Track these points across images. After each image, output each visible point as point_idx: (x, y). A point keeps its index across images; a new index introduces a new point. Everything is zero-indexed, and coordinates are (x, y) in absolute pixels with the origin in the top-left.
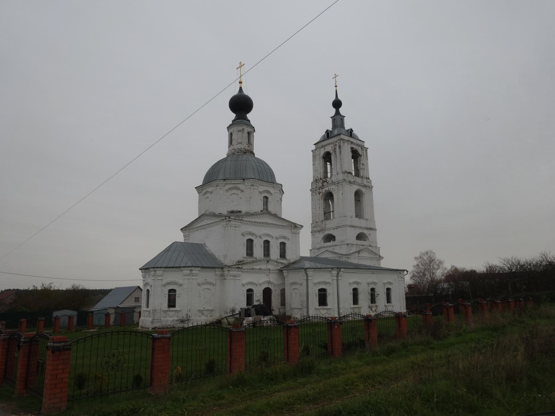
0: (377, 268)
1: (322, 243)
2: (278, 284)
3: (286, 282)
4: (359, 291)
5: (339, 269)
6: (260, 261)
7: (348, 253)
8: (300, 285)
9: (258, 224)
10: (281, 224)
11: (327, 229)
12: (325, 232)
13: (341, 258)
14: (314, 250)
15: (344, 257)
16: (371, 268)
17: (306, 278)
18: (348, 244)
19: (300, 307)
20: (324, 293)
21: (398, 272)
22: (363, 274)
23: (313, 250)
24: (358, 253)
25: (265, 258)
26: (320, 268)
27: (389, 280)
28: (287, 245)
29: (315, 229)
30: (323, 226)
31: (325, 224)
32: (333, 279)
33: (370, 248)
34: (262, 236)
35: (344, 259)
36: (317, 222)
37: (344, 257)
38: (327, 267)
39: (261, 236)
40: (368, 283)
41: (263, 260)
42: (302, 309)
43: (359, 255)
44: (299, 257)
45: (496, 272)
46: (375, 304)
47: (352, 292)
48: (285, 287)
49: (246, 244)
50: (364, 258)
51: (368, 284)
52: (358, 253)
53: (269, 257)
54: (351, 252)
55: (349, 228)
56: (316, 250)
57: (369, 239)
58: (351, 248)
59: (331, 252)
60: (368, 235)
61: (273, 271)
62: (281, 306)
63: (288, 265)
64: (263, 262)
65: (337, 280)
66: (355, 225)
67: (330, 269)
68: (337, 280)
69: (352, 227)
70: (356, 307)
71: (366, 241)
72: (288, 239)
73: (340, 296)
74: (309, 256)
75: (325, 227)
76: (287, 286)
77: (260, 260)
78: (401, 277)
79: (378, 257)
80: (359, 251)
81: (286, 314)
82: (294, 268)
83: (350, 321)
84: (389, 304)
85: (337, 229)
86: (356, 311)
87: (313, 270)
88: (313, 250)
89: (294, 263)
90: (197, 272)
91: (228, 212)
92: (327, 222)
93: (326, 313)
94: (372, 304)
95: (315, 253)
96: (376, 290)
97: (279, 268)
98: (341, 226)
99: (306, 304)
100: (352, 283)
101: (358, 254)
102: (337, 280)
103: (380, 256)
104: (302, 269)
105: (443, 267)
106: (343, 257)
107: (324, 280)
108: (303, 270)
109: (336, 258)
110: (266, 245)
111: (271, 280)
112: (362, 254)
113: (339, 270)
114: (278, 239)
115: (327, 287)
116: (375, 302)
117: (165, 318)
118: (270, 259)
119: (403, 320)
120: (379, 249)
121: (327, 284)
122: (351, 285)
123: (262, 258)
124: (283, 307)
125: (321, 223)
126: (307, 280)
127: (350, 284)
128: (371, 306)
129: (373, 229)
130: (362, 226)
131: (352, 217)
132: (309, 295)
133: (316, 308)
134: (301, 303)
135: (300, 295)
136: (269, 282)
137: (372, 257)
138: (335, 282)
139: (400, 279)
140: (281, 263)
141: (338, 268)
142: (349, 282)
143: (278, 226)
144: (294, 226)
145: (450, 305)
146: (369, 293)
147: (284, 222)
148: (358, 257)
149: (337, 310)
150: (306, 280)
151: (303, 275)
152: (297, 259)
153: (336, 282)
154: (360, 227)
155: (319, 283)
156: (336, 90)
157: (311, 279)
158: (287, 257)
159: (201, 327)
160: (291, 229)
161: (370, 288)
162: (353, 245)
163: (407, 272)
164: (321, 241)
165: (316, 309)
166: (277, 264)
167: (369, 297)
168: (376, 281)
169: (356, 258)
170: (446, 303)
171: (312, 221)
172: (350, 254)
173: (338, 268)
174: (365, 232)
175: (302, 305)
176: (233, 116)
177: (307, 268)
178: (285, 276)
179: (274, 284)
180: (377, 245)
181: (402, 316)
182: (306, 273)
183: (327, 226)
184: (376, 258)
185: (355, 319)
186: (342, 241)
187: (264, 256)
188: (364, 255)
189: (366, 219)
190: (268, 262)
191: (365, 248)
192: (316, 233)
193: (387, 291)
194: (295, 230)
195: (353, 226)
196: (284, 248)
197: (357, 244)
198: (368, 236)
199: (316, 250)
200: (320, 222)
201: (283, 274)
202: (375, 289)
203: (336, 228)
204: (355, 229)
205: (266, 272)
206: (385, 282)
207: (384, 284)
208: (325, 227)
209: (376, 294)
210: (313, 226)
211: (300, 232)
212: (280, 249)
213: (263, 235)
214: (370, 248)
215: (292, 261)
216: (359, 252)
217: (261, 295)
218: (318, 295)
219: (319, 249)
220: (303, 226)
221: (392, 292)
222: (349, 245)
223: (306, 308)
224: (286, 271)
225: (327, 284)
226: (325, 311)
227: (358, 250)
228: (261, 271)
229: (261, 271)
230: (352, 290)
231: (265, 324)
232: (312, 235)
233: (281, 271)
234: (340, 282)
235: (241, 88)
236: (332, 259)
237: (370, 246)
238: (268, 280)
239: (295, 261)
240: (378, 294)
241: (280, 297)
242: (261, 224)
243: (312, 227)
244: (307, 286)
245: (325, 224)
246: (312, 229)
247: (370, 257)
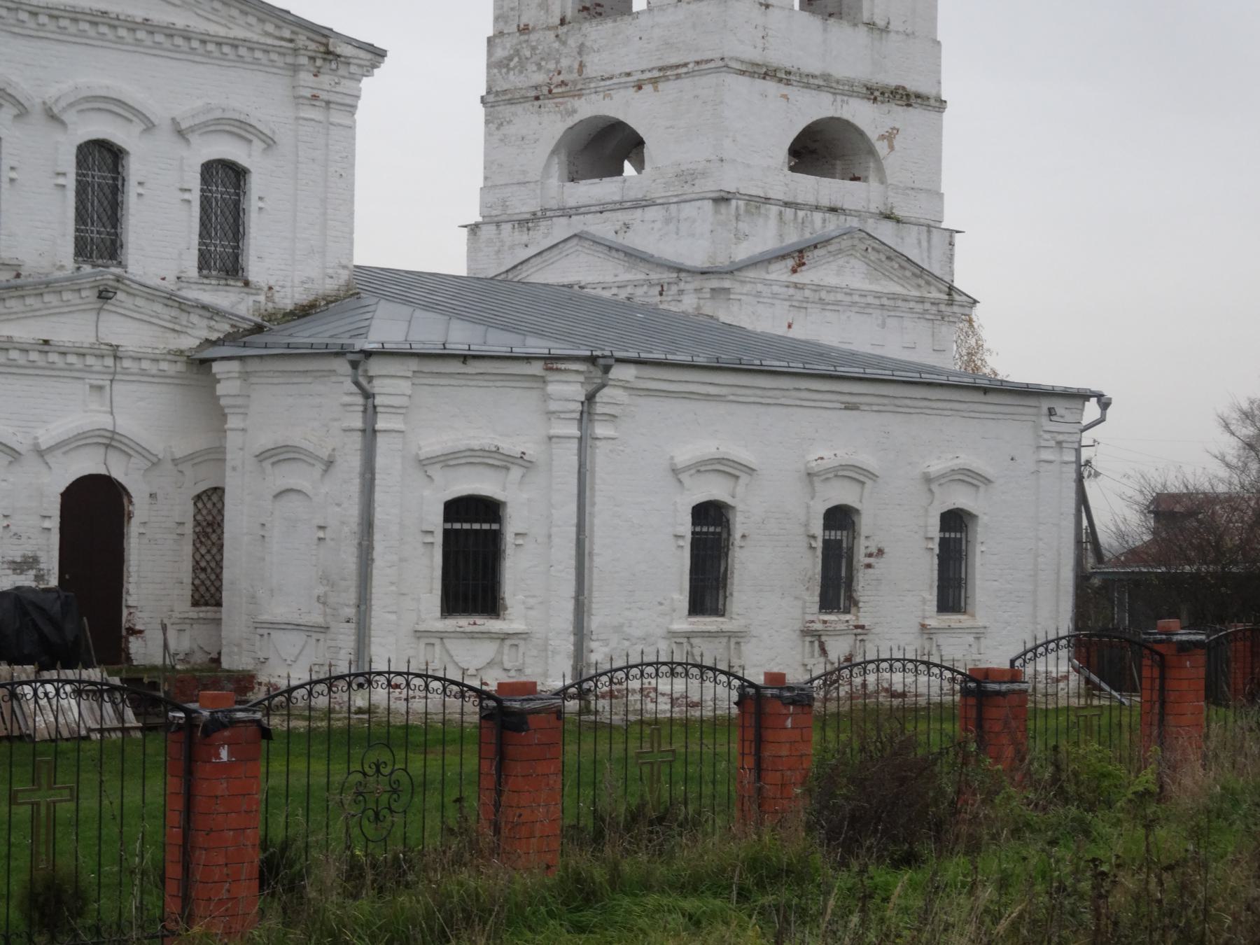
0: (886, 374)
1: (554, 182)
2: (178, 454)
3: (233, 441)
4: (740, 525)
5: (599, 364)
6: (45, 286)
7: (722, 261)
8: (320, 467)
9: (43, 19)
10: (213, 29)
11: (591, 79)
12: (577, 103)
13: (674, 289)
14: (493, 227)
15: (690, 284)
16: (842, 370)
17: (359, 424)
18: (722, 199)
19: (316, 618)
20: (486, 526)
21: (1032, 401)
22: (772, 409)
23: (488, 232)
24: (790, 263)
25: (87, 268)
26: (465, 358)
27: (967, 459)
28: (256, 185)
29: (515, 80)
30: (565, 63)
31: (581, 49)
32: (550, 438)
33: (885, 231)
34: (64, 110)
35: (688, 303)
36: (524, 30)
37: (689, 287)
38: (518, 351)
39: (55, 110)
40: (809, 474)
41: (73, 285)
42: (325, 629)
43: (796, 278)
44: (344, 275)
46: (848, 617)
47: (686, 527)
48: (224, 477)
49: (71, 182)
50: (831, 297)
51: (811, 483)
52: (790, 263)
53: (120, 264)
54: (742, 252)
55: (745, 80)
56: (507, 228)
57: (880, 170)
58: (744, 226)
59: (610, 248)
60: (882, 137)
61: (145, 365)
62: (195, 604)
63: (259, 329)
64: (67, 296)
65: (584, 443)
66: (787, 63)
67: (536, 368)
68: (584, 443)
69: (765, 76)
70: (713, 628)
71: (866, 180)
72: (270, 143)
73: (597, 550)
74: (464, 273)
75: (580, 72)
76: (234, 469)
77: (48, 284)
78: (1059, 443)
79: (935, 294)
80: (801, 251)
81: (226, 664)
82: (288, 346)
83: (656, 721)
84: (952, 619)
85: (661, 86)
86: (709, 652)
87: (413, 365)
88: (488, 232)
89: (304, 312)
90: (405, 386)
92: (597, 32)
93: (490, 664)
94: (826, 617)
95: (499, 251)
96: (865, 524)
97: (188, 342)
98: (685, 65)
99: (351, 596)
100: (688, 468)
101: (794, 271)
102: (580, 439)
103: (951, 289)
104: (337, 354)
106: (682, 285)
107: (481, 438)
108: (343, 366)
109: (640, 291)
110: (218, 191)
111: (127, 425)
112: (820, 273)
113: (599, 374)
114: (187, 141)
115: (504, 489)
116: (852, 603)
118: (118, 279)
119: (789, 723)
120: (951, 244)
121: (508, 469)
122: (680, 482)
123: (62, 267)
124: (206, 612)
125: (551, 35)
126: (370, 433)
127: (675, 471)
128: (818, 626)
129: (918, 96)
130: (841, 71)
131: (767, 6)
132: (377, 537)
133: (422, 627)
134: (320, 590)
135: (321, 534)
136: (111, 441)
137: (893, 297)
138: (568, 456)
139: (1046, 455)
140: (205, 307)
141: (592, 360)
142: (672, 458)
143: (195, 44)
144: (313, 46)
145: (1183, 636)
146: (814, 537)
147: (241, 20)
148: (791, 291)
149: (568, 645)
150: (364, 431)
151: (347, 399)
152: (329, 286)
153: (574, 460)
154: (826, 77)
155: (449, 460)
157: (400, 426)
158: (256, 269)
160: (295, 68)
161: (820, 508)
162: (759, 202)
163: (1104, 404)
164: (547, 166)
165: (419, 634)
166: (174, 313)
167: (813, 565)
168: (867, 459)
169: (775, 296)
170: (1162, 623)
171: (497, 19)
172: (733, 270)
173: (592, 360)
174: (861, 114)
175: (324, 603)
177: (368, 354)
178: (223, 402)
179: (143, 452)
180: (941, 212)
181: (779, 697)
182: (357, 383)
183: (596, 65)
184: (921, 300)
185: (696, 713)
186: (687, 176)
187: (83, 250)
188: (832, 280)
189: (871, 25)
190: (104, 295)
191: (848, 233)
192: (513, 108)
193: (942, 529)
194: (326, 80)
195: (769, 73)
196: (237, 204)
197: (790, 199)
198: (881, 148)
199: (507, 228)
200: (549, 28)
201: (214, 389)
202: (857, 511)
203: (654, 81)
204: (784, 89)
205: (88, 369)
206: (937, 466)
207: (928, 479)
208: (580, 72)
209: (862, 547)
210: (500, 53)
211: (358, 97)
212: (203, 208)
213: (71, 105)
214: (885, 231)
215: (288, 299)
216: (799, 256)
217: (47, 524)
218: (438, 539)
219: (526, 223)
220: (379, 54)
221: (980, 538)
222: (734, 202)
223: (353, 625)
224: (235, 366)
225: (508, 469)
226: (487, 650)
227: (793, 238)
228: (53, 357)
229: (53, 357)
230: (689, 519)
231: (40, 723)
232: (487, 122)
233: (204, 364)
234: (601, 458)
236: (607, 294)
237: (888, 217)
238: (104, 421)
239: (312, 298)
240: (881, 552)
241: (188, 549)
242: (63, 23)
243: (489, 66)
245: (581, 49)
246: (488, 73)
247: (878, 296)
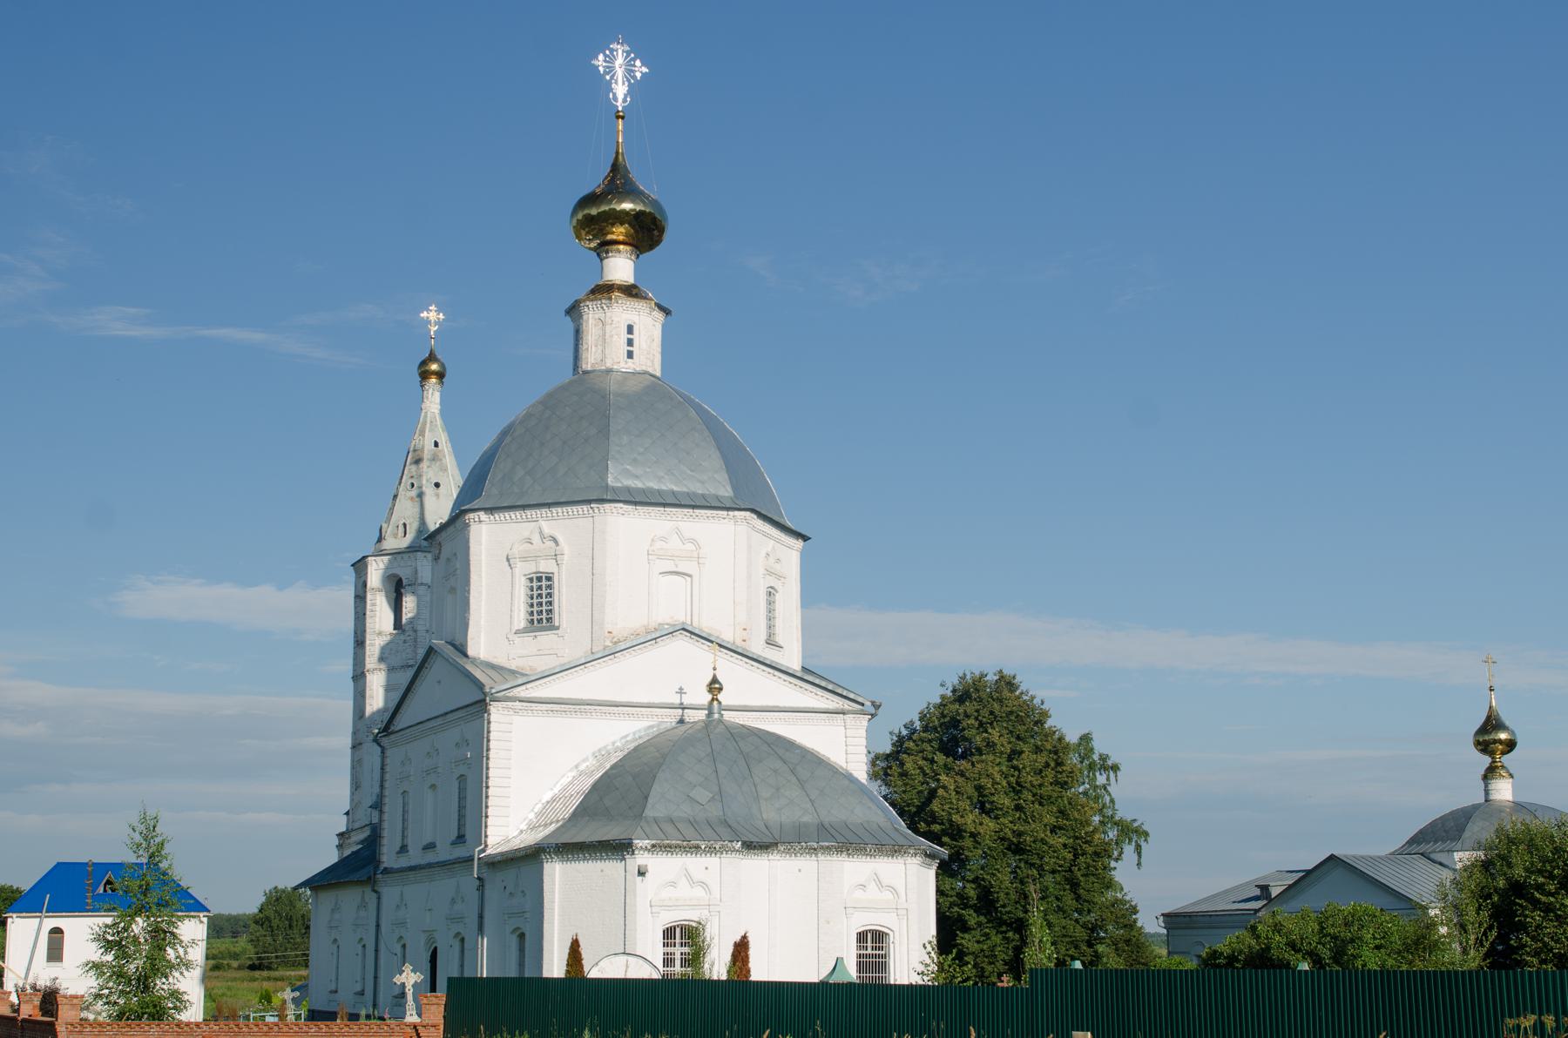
45: (1504, 972)
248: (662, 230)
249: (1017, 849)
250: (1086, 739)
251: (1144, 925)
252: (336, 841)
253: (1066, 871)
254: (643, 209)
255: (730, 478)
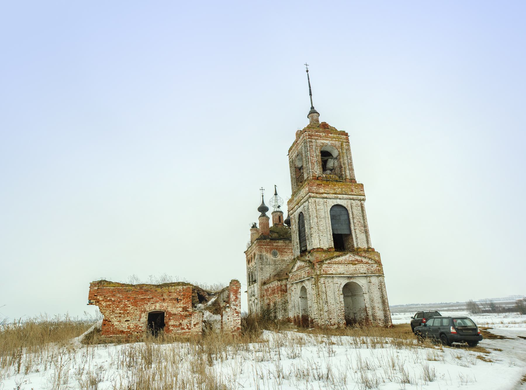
45: (271, 224)
91: (252, 227)
105: (296, 357)
117: (297, 339)
137: (452, 307)
156: (308, 74)
159: (354, 179)
176: (260, 213)
235: (313, 112)
244: (523, 337)
248: (268, 211)
249: (334, 189)
250: (89, 287)
251: (211, 285)
252: (89, 285)
253: (313, 284)
254: (348, 281)
255: (132, 286)
